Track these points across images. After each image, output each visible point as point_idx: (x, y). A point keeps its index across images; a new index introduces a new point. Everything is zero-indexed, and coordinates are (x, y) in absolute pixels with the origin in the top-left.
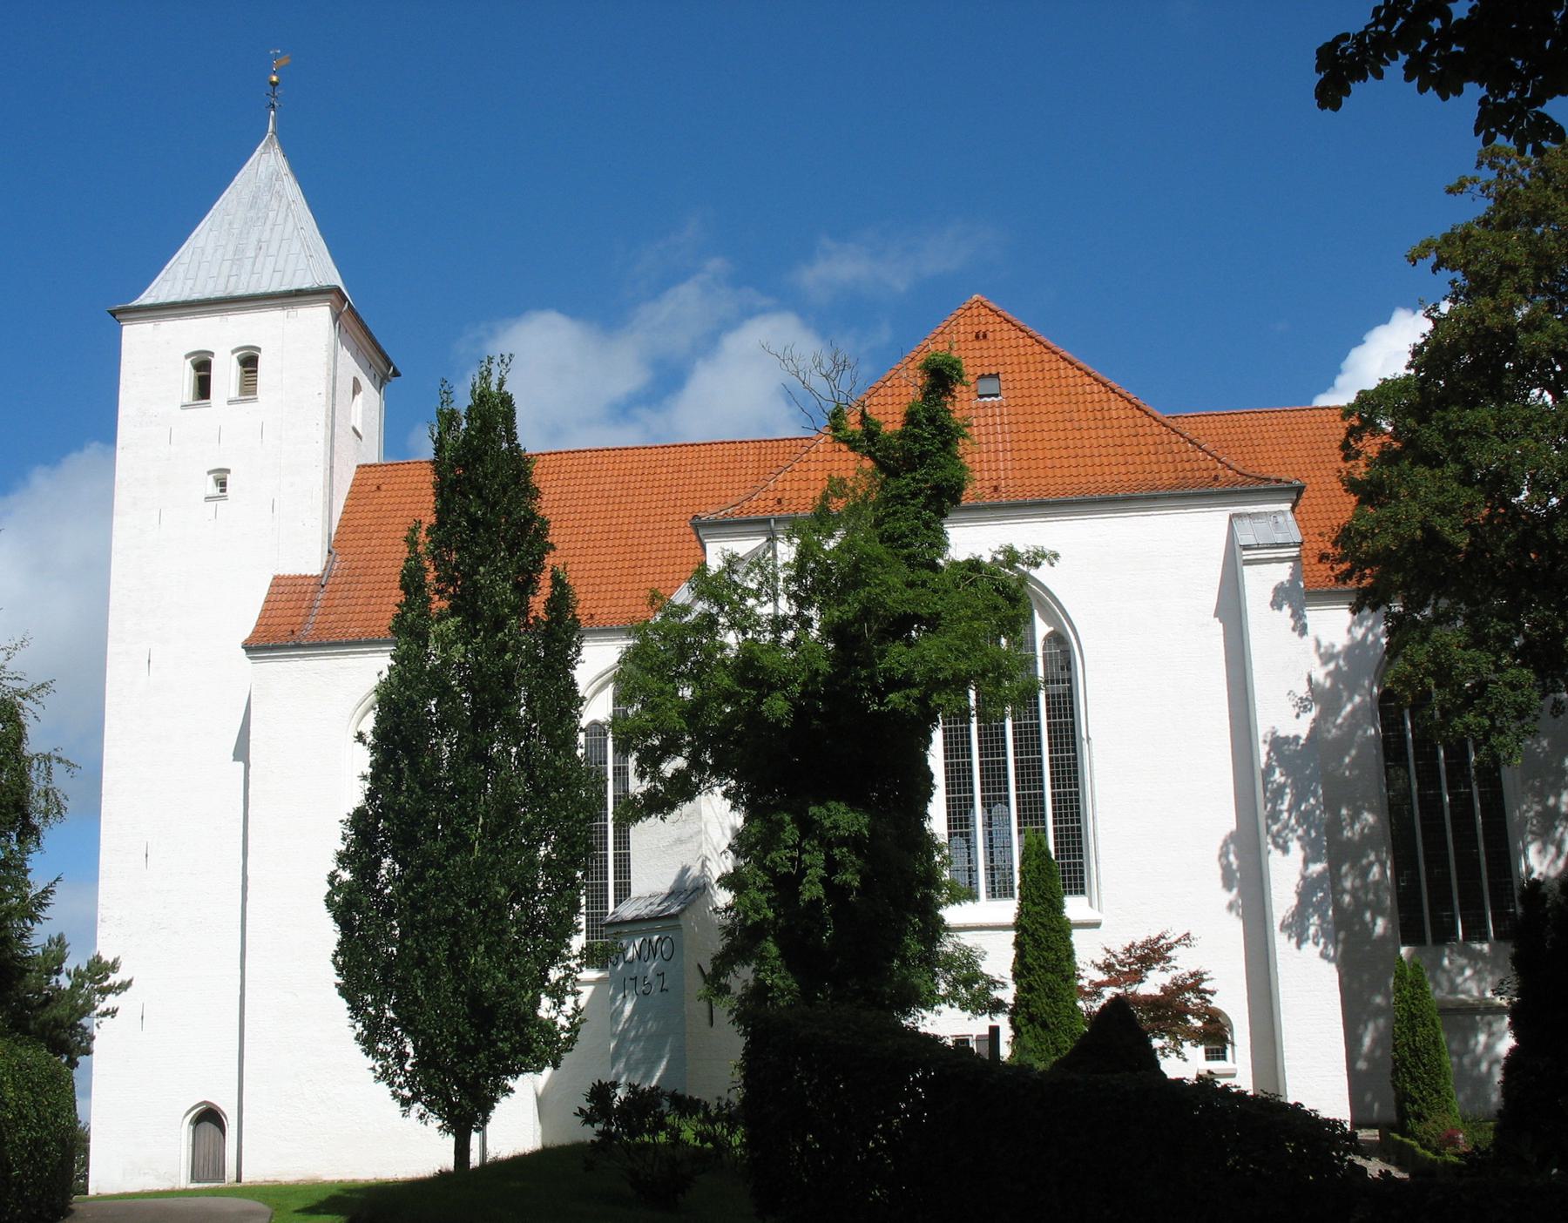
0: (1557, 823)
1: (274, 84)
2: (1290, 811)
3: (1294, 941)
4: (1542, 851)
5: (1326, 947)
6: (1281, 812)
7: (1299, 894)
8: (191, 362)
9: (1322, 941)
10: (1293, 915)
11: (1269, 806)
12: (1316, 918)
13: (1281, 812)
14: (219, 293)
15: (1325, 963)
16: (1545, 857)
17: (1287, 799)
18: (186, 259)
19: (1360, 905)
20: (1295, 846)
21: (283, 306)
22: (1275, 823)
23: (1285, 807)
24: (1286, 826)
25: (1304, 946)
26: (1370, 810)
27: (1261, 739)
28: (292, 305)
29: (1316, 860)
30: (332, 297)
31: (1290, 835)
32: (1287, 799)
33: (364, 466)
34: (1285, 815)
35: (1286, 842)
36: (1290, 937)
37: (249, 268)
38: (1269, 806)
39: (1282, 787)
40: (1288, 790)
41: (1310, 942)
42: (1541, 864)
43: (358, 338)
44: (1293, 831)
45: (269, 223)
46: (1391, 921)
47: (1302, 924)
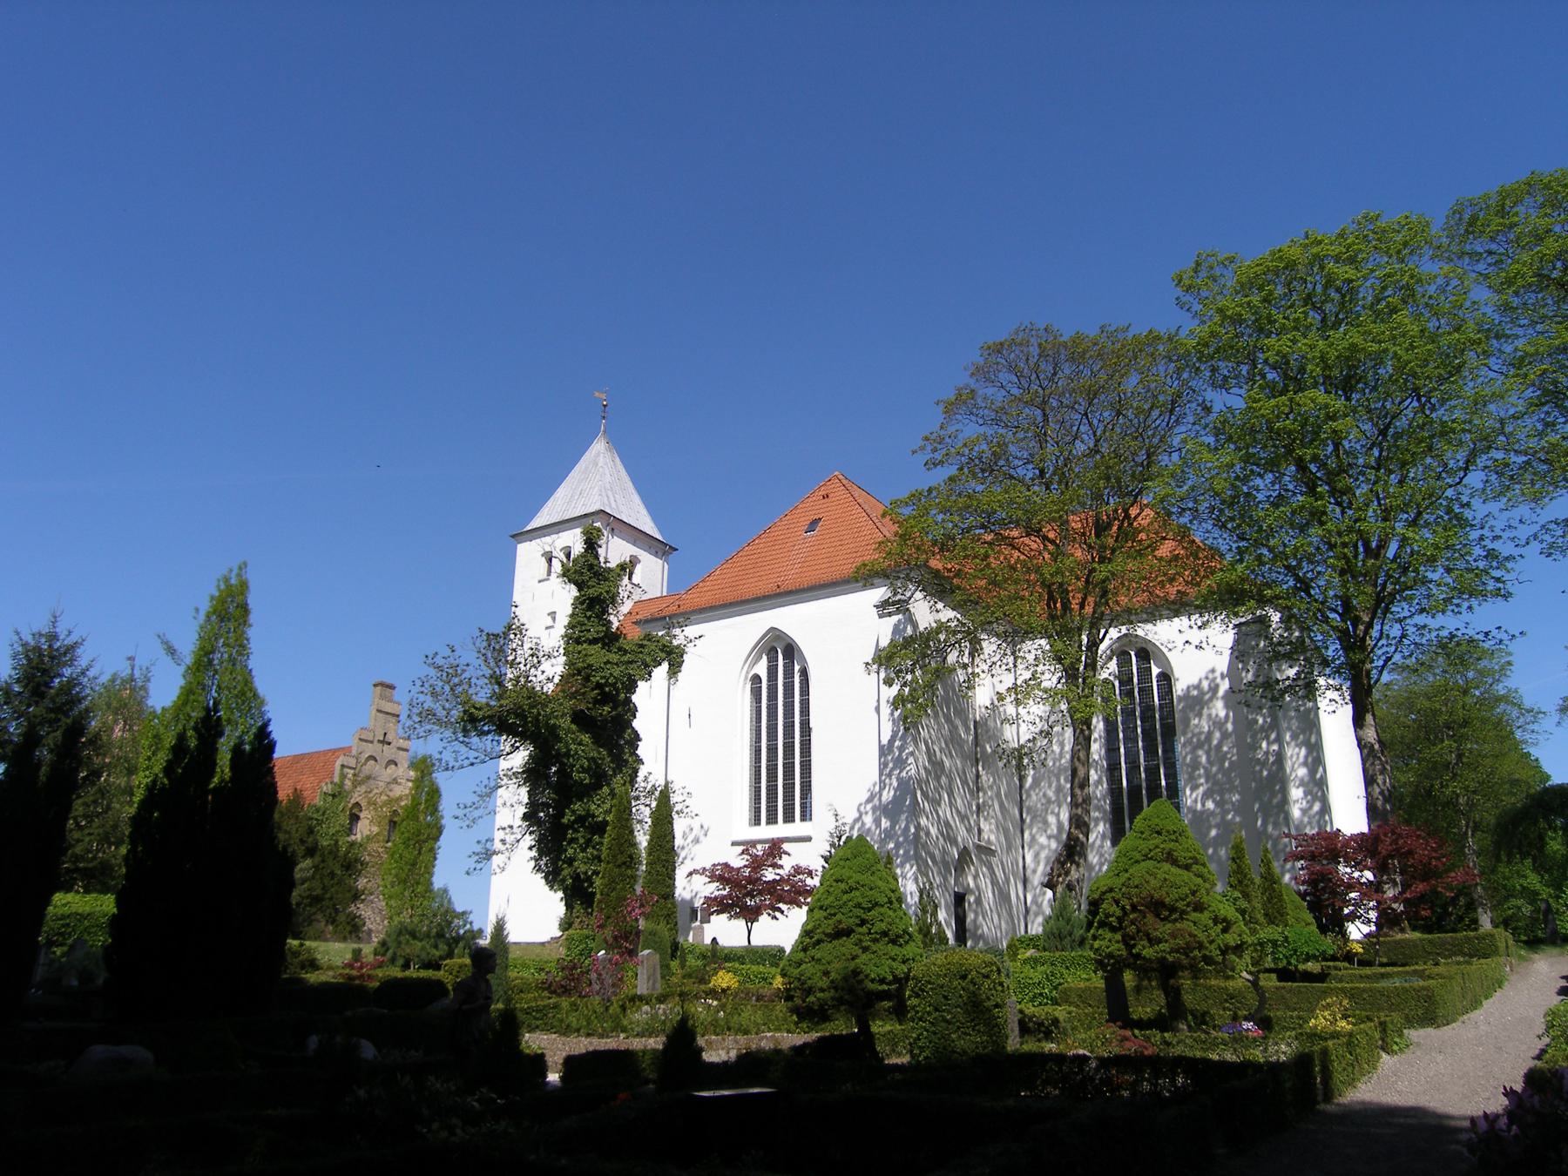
1: (605, 406)
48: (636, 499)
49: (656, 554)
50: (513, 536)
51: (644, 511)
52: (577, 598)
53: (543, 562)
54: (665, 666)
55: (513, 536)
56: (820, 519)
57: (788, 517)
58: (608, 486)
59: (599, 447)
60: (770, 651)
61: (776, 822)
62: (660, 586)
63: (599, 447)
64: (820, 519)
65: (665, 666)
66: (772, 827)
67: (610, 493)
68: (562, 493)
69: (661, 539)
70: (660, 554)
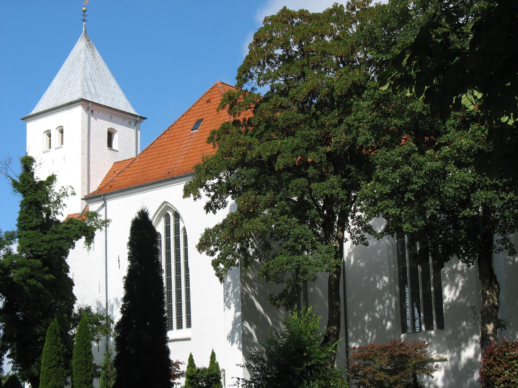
0: (456, 275)
1: (84, 11)
2: (231, 292)
3: (230, 343)
4: (450, 289)
5: (239, 345)
6: (229, 293)
7: (233, 324)
8: (59, 131)
9: (239, 342)
10: (231, 333)
11: (226, 291)
12: (237, 333)
13: (229, 293)
14: (53, 106)
15: (239, 350)
16: (451, 291)
17: (231, 288)
18: (48, 93)
19: (382, 317)
20: (233, 306)
21: (68, 108)
22: (227, 298)
23: (230, 291)
24: (230, 298)
25: (233, 345)
26: (386, 276)
27: (165, 272)
28: (71, 108)
29: (238, 311)
30: (81, 102)
31: (231, 302)
32: (231, 288)
33: (115, 163)
34: (230, 294)
35: (230, 304)
36: (229, 341)
37: (64, 93)
38: (226, 291)
39: (230, 283)
40: (231, 285)
41: (235, 343)
42: (450, 294)
43: (105, 111)
44: (232, 300)
45: (74, 72)
46: (393, 323)
47: (233, 336)
48: (113, 82)
49: (129, 125)
50: (23, 119)
51: (119, 91)
52: (22, 202)
53: (46, 136)
54: (83, 239)
55: (23, 119)
56: (202, 119)
57: (184, 117)
58: (88, 76)
59: (81, 44)
60: (166, 216)
61: (182, 328)
62: (134, 147)
63: (81, 44)
64: (202, 119)
65: (83, 239)
66: (180, 331)
67: (90, 82)
68: (57, 82)
69: (133, 112)
70: (133, 123)
